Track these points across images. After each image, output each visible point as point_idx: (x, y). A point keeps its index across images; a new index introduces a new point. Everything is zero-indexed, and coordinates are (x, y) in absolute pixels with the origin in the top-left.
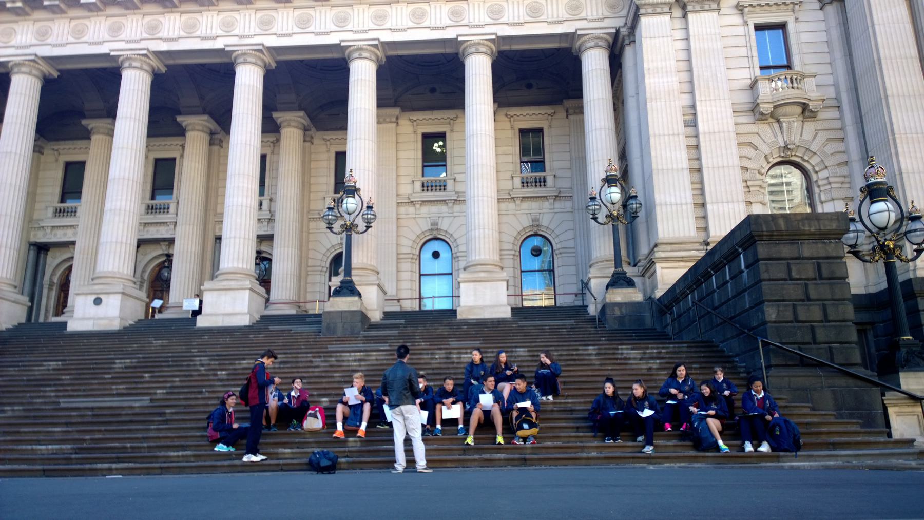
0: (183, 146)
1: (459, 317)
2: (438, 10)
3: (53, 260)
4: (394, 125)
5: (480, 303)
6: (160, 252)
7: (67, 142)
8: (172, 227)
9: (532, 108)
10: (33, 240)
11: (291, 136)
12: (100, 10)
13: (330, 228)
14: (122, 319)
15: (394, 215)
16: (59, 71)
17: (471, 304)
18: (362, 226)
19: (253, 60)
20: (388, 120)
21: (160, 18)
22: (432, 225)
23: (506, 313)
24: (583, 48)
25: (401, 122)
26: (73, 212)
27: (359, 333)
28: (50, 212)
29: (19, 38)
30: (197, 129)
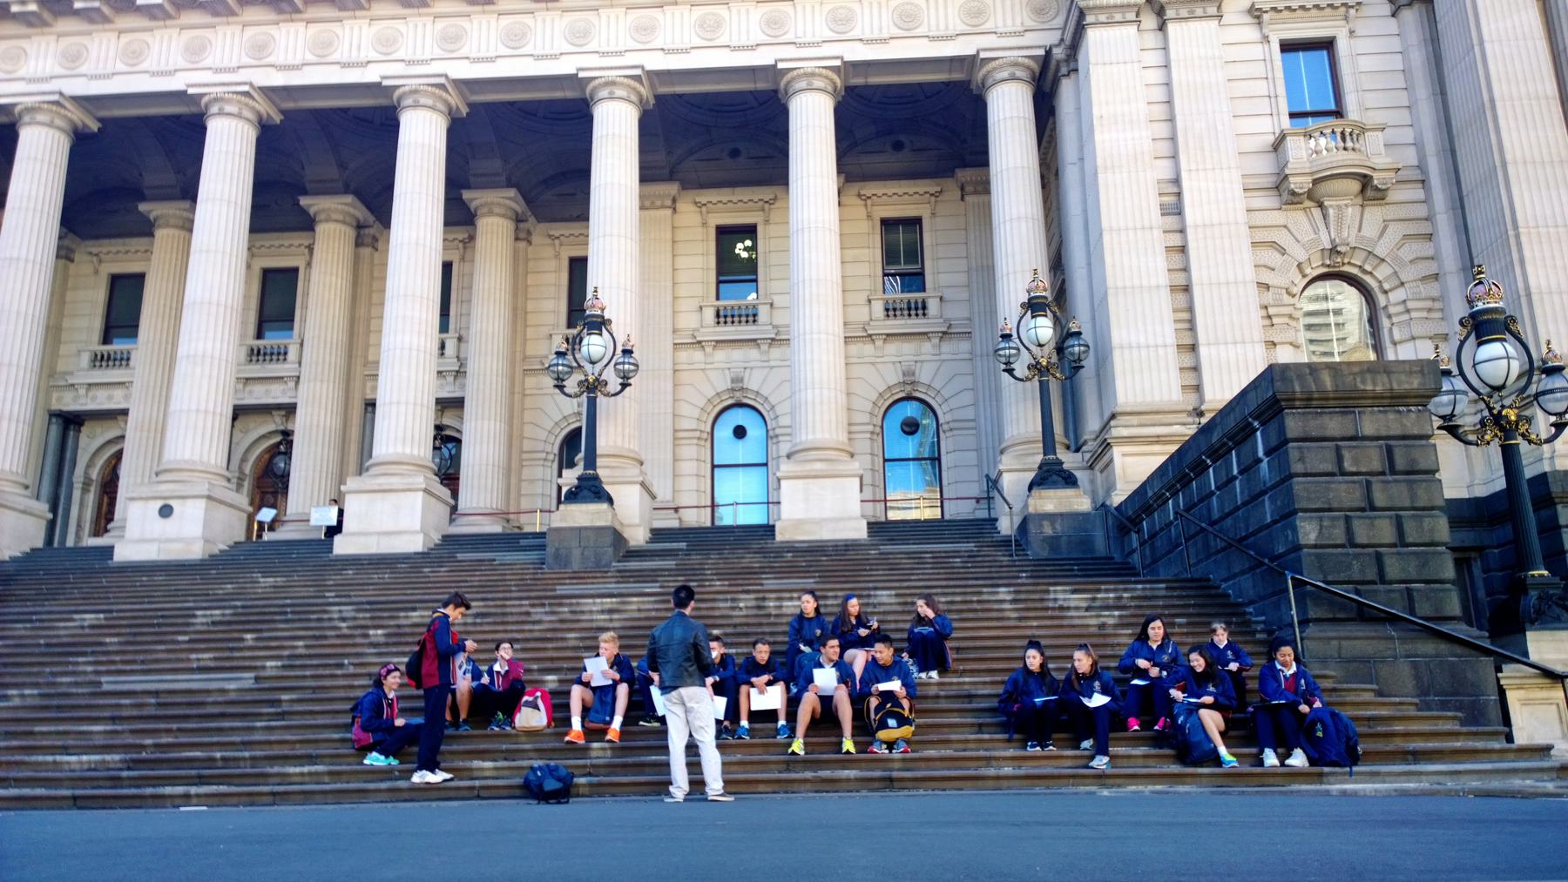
0: (310, 248)
1: (779, 537)
2: (743, 17)
3: (90, 440)
4: (669, 212)
5: (815, 514)
6: (271, 427)
7: (113, 241)
8: (292, 384)
9: (903, 182)
10: (55, 406)
11: (494, 231)
12: (168, 16)
13: (561, 387)
14: (206, 541)
15: (669, 365)
16: (100, 120)
17: (800, 516)
18: (614, 383)
19: (430, 102)
20: (659, 203)
21: (272, 30)
22: (733, 381)
23: (859, 532)
24: (990, 81)
25: (680, 206)
26: (124, 360)
27: (608, 565)
28: (85, 359)
29: (32, 63)
30: (334, 218)
